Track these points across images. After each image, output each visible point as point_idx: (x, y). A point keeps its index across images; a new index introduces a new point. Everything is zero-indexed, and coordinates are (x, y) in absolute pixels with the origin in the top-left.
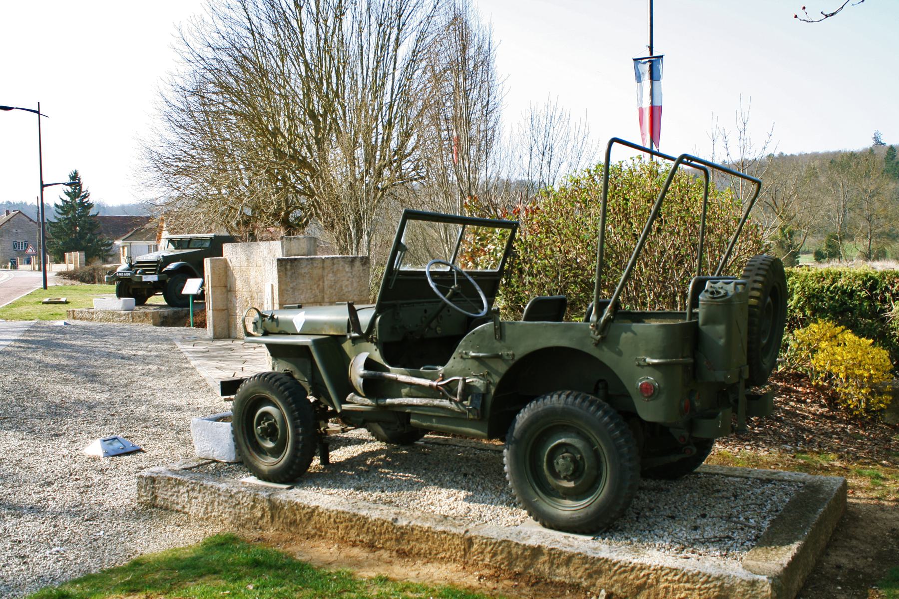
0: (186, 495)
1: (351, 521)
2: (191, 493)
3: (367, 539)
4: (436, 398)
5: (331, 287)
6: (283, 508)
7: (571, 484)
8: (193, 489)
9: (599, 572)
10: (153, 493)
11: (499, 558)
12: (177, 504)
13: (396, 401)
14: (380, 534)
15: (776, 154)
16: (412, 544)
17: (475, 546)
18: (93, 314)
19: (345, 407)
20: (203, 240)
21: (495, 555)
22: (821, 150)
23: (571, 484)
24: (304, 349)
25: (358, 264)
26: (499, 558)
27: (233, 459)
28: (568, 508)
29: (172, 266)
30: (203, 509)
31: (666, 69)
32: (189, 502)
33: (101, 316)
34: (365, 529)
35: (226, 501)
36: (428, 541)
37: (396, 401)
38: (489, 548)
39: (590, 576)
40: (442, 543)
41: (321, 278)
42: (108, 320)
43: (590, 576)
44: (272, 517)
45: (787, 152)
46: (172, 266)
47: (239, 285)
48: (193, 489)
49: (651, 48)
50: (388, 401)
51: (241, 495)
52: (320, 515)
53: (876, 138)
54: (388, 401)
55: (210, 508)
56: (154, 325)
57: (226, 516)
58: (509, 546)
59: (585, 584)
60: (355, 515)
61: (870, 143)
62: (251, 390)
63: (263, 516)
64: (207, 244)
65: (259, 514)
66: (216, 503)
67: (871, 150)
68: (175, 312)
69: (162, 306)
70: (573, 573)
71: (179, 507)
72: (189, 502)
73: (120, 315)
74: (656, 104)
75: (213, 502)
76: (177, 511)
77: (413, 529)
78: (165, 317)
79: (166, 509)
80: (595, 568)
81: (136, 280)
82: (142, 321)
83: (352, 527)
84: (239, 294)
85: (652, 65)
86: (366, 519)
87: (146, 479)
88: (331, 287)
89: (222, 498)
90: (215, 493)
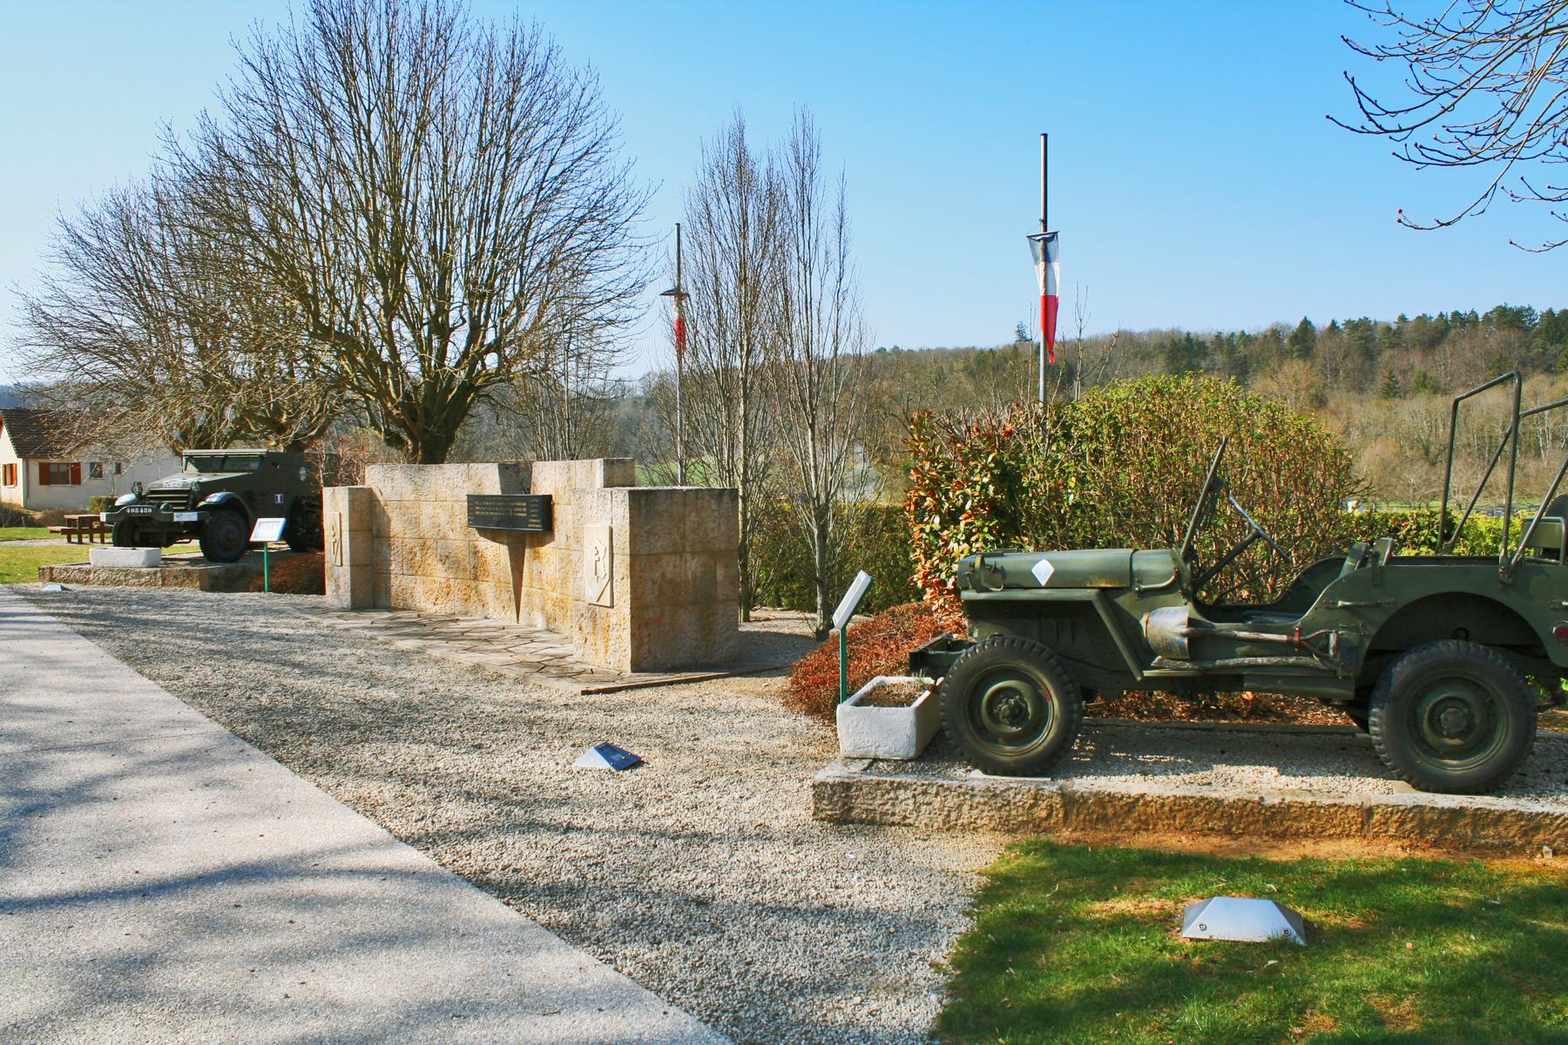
0: (911, 802)
1: (1197, 806)
2: (920, 799)
3: (1219, 825)
4: (1290, 655)
5: (694, 531)
6: (1085, 802)
7: (1457, 741)
8: (925, 793)
9: (1537, 829)
10: (845, 804)
11: (1409, 826)
12: (893, 814)
13: (1232, 662)
14: (1241, 817)
15: (889, 348)
16: (1287, 824)
17: (1376, 817)
18: (88, 572)
19: (1147, 673)
20: (247, 459)
21: (1402, 823)
22: (950, 345)
23: (1457, 741)
24: (1086, 605)
25: (726, 499)
26: (1409, 826)
27: (912, 754)
28: (1455, 767)
29: (214, 498)
30: (940, 819)
31: (1060, 248)
32: (917, 809)
33: (103, 576)
34: (1218, 814)
35: (985, 803)
36: (1310, 817)
37: (1232, 662)
38: (1395, 817)
39: (1525, 834)
40: (1331, 817)
41: (682, 518)
42: (119, 583)
43: (1525, 834)
44: (1066, 816)
45: (904, 347)
46: (214, 498)
47: (397, 527)
48: (925, 793)
49: (1045, 222)
50: (1218, 662)
51: (1011, 793)
52: (1146, 804)
53: (1020, 332)
54: (1218, 662)
55: (953, 815)
56: (202, 589)
57: (985, 821)
58: (1421, 812)
59: (1519, 843)
60: (1202, 799)
61: (1012, 339)
62: (987, 660)
63: (1049, 815)
64: (255, 466)
65: (1044, 814)
66: (966, 808)
67: (1015, 348)
68: (228, 570)
69: (194, 561)
70: (1503, 833)
71: (896, 819)
72: (917, 809)
73: (139, 575)
74: (1050, 293)
75: (960, 806)
76: (893, 824)
77: (1289, 806)
78: (216, 578)
79: (872, 822)
80: (1532, 824)
81: (162, 520)
82: (181, 584)
83: (1197, 814)
84: (396, 542)
85: (1046, 243)
86: (1219, 802)
87: (832, 786)
88: (694, 531)
89: (976, 800)
90: (964, 794)
